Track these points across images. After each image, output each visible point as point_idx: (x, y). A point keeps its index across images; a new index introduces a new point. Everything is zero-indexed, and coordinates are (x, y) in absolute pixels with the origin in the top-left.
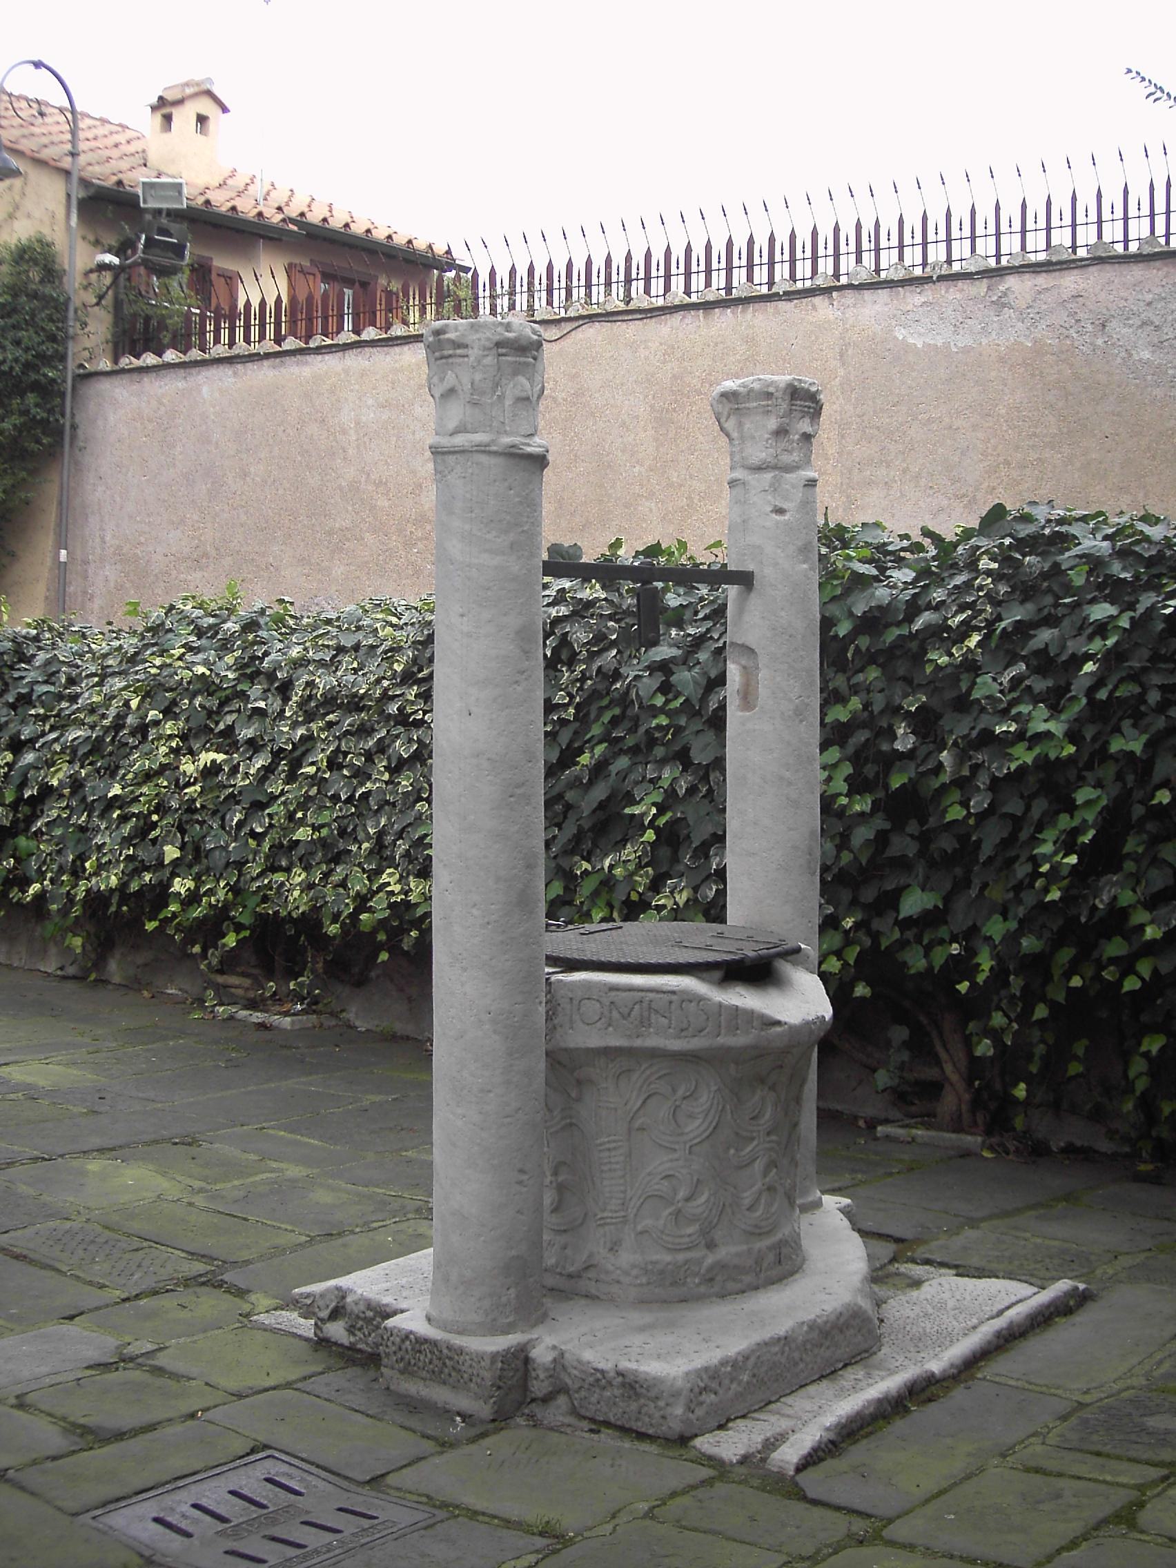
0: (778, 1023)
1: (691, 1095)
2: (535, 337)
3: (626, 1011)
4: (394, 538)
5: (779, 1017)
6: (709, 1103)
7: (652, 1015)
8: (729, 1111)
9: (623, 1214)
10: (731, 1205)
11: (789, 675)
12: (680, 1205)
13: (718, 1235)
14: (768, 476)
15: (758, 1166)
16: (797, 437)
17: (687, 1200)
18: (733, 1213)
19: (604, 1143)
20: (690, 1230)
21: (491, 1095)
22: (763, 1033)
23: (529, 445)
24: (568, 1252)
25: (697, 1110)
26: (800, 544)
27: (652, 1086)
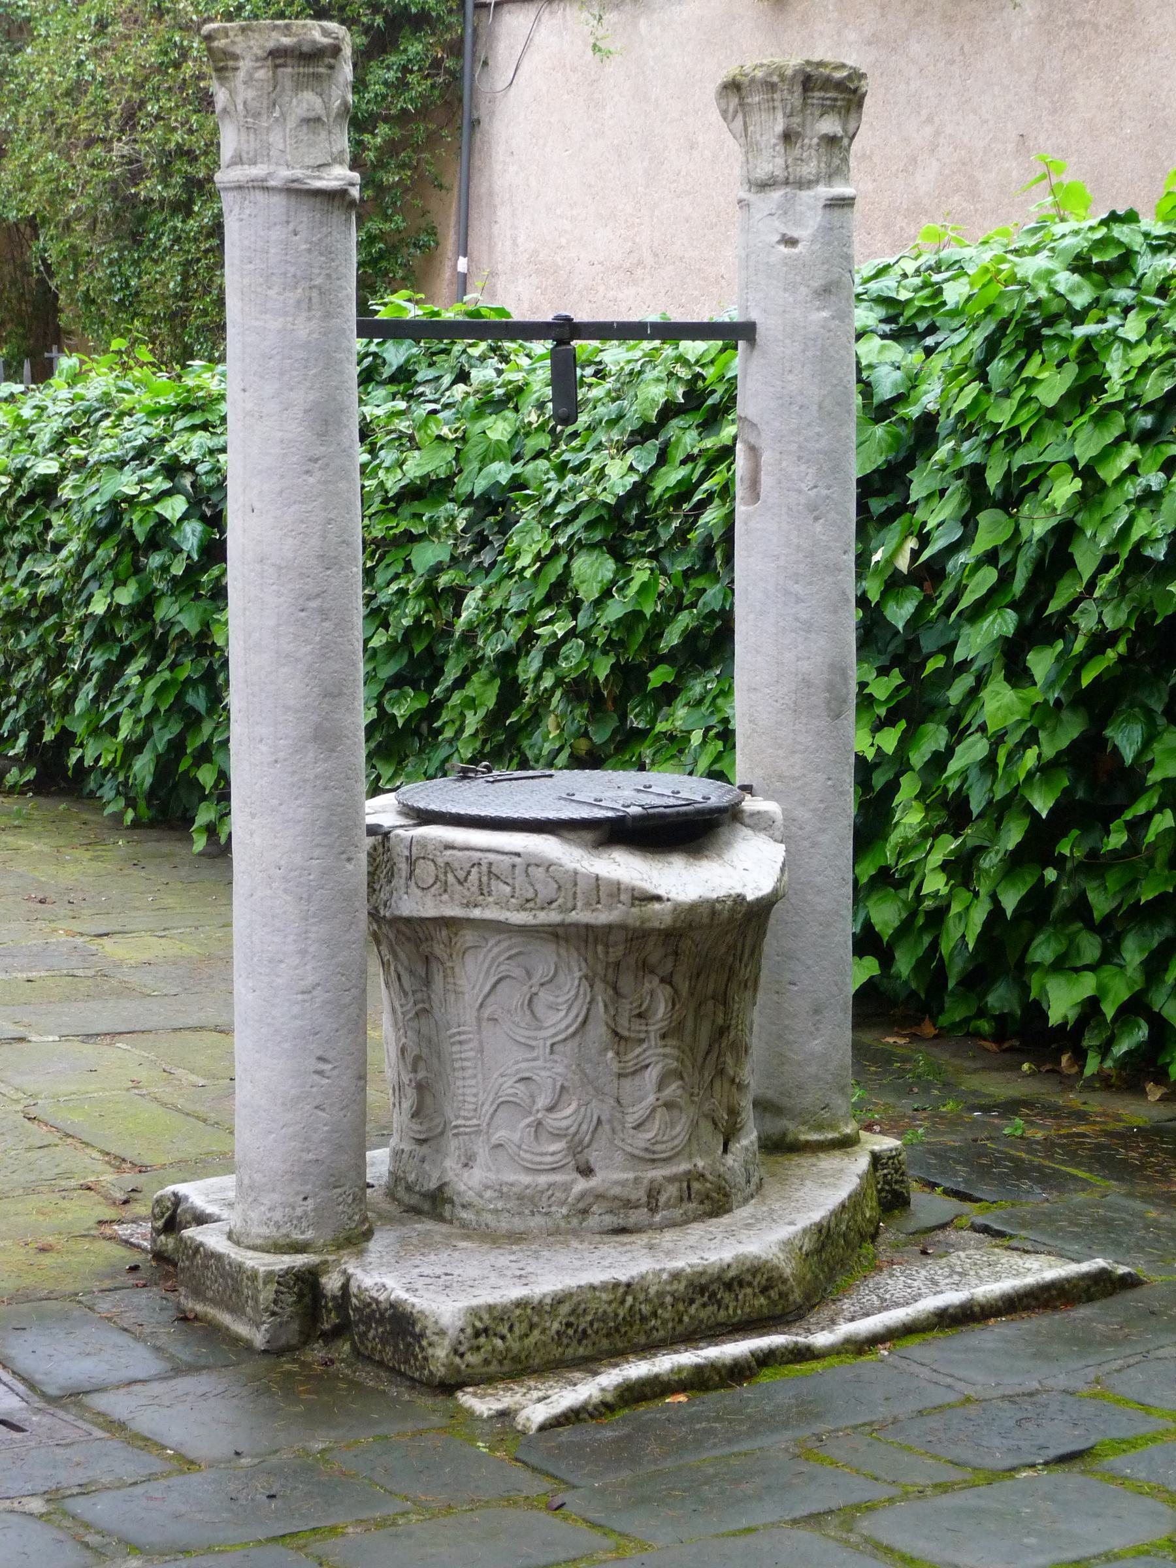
0: (658, 898)
1: (551, 981)
2: (326, 41)
3: (461, 874)
4: (879, 237)
5: (661, 892)
6: (573, 992)
7: (493, 882)
8: (601, 1005)
9: (475, 1122)
10: (610, 1121)
11: (799, 458)
12: (540, 1115)
13: (594, 1157)
14: (777, 195)
15: (651, 1075)
16: (815, 140)
17: (550, 1109)
18: (614, 1131)
19: (454, 1035)
20: (553, 1148)
21: (283, 966)
22: (633, 910)
23: (320, 178)
24: (426, 1166)
25: (560, 1000)
26: (816, 284)
27: (502, 968)
